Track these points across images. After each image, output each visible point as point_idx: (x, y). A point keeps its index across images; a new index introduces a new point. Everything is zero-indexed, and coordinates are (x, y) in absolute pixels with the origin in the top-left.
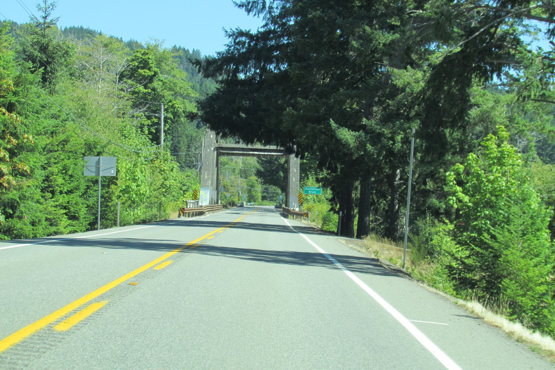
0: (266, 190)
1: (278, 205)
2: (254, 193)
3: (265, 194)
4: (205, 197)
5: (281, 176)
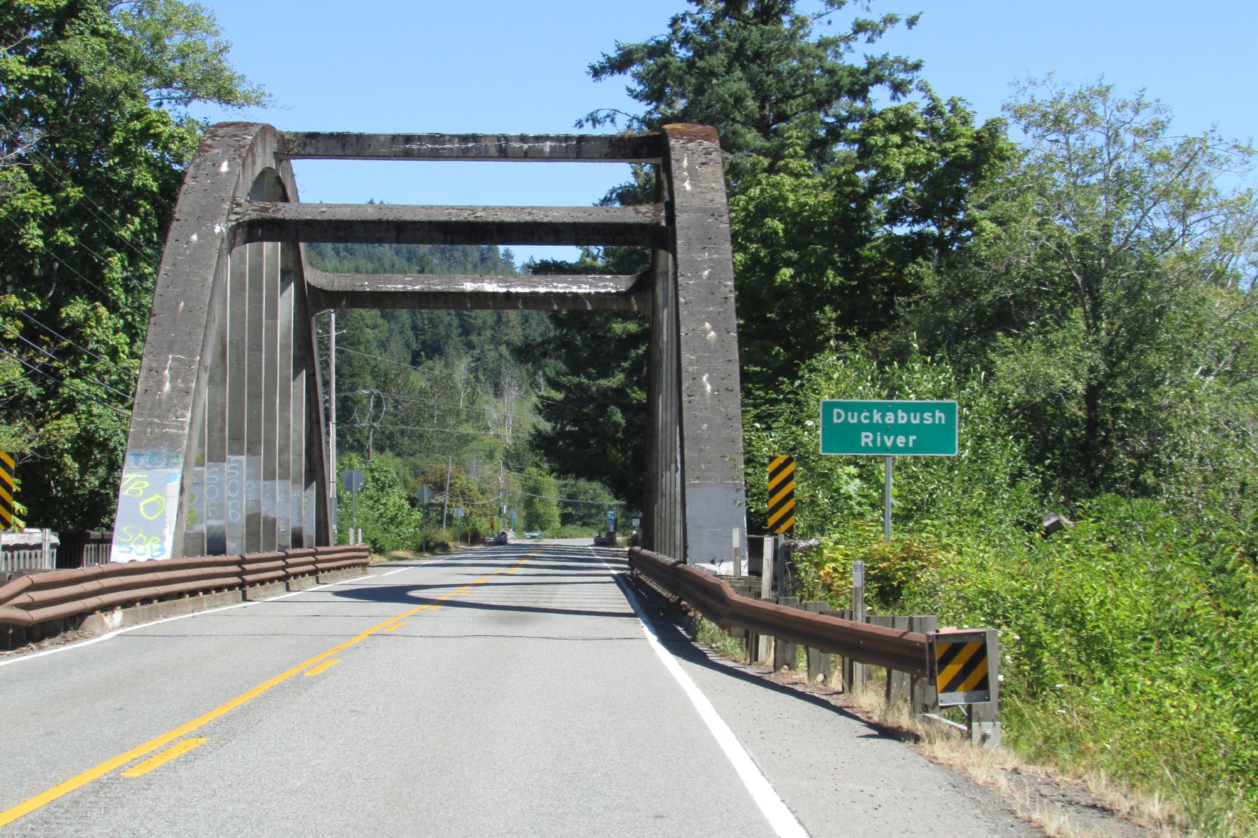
0: (570, 501)
1: (604, 535)
2: (540, 508)
3: (570, 509)
4: (151, 508)
5: (617, 425)
